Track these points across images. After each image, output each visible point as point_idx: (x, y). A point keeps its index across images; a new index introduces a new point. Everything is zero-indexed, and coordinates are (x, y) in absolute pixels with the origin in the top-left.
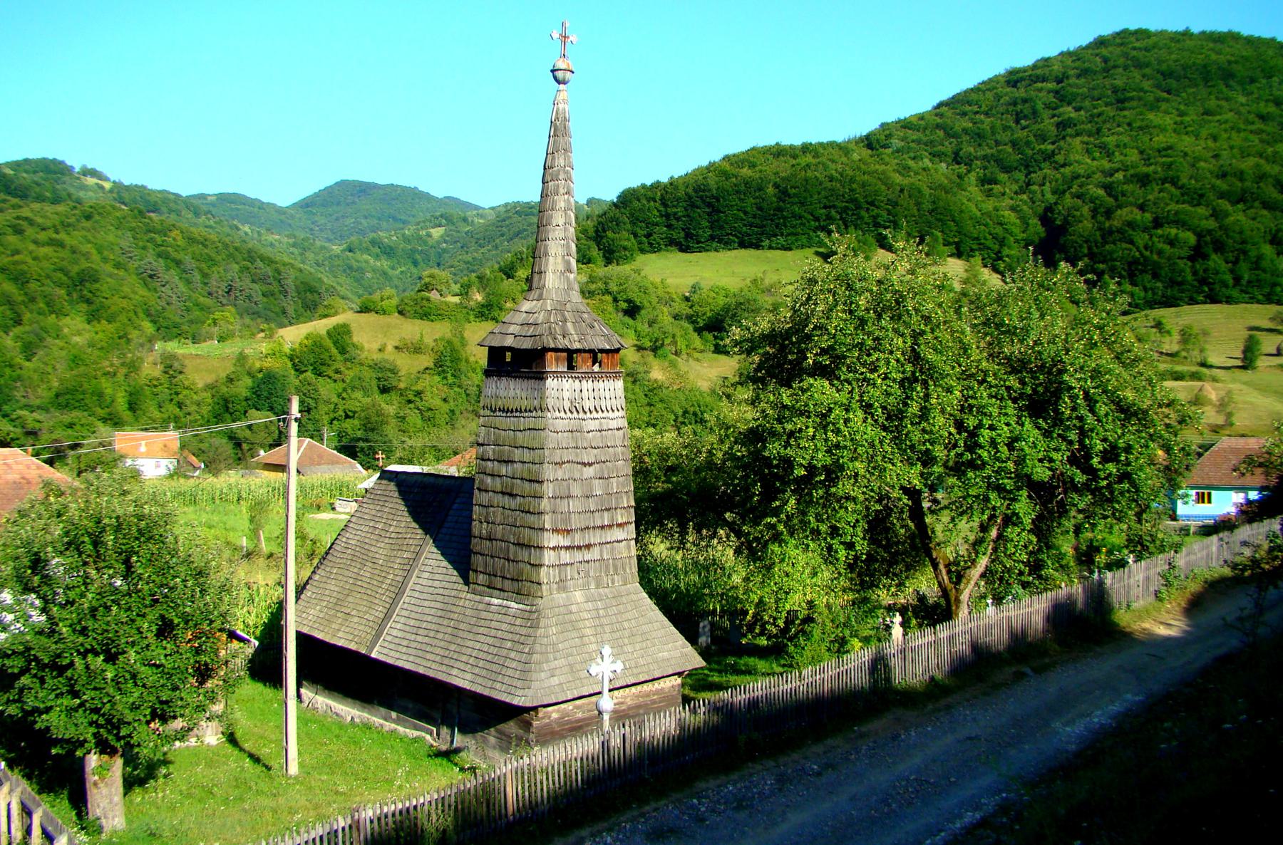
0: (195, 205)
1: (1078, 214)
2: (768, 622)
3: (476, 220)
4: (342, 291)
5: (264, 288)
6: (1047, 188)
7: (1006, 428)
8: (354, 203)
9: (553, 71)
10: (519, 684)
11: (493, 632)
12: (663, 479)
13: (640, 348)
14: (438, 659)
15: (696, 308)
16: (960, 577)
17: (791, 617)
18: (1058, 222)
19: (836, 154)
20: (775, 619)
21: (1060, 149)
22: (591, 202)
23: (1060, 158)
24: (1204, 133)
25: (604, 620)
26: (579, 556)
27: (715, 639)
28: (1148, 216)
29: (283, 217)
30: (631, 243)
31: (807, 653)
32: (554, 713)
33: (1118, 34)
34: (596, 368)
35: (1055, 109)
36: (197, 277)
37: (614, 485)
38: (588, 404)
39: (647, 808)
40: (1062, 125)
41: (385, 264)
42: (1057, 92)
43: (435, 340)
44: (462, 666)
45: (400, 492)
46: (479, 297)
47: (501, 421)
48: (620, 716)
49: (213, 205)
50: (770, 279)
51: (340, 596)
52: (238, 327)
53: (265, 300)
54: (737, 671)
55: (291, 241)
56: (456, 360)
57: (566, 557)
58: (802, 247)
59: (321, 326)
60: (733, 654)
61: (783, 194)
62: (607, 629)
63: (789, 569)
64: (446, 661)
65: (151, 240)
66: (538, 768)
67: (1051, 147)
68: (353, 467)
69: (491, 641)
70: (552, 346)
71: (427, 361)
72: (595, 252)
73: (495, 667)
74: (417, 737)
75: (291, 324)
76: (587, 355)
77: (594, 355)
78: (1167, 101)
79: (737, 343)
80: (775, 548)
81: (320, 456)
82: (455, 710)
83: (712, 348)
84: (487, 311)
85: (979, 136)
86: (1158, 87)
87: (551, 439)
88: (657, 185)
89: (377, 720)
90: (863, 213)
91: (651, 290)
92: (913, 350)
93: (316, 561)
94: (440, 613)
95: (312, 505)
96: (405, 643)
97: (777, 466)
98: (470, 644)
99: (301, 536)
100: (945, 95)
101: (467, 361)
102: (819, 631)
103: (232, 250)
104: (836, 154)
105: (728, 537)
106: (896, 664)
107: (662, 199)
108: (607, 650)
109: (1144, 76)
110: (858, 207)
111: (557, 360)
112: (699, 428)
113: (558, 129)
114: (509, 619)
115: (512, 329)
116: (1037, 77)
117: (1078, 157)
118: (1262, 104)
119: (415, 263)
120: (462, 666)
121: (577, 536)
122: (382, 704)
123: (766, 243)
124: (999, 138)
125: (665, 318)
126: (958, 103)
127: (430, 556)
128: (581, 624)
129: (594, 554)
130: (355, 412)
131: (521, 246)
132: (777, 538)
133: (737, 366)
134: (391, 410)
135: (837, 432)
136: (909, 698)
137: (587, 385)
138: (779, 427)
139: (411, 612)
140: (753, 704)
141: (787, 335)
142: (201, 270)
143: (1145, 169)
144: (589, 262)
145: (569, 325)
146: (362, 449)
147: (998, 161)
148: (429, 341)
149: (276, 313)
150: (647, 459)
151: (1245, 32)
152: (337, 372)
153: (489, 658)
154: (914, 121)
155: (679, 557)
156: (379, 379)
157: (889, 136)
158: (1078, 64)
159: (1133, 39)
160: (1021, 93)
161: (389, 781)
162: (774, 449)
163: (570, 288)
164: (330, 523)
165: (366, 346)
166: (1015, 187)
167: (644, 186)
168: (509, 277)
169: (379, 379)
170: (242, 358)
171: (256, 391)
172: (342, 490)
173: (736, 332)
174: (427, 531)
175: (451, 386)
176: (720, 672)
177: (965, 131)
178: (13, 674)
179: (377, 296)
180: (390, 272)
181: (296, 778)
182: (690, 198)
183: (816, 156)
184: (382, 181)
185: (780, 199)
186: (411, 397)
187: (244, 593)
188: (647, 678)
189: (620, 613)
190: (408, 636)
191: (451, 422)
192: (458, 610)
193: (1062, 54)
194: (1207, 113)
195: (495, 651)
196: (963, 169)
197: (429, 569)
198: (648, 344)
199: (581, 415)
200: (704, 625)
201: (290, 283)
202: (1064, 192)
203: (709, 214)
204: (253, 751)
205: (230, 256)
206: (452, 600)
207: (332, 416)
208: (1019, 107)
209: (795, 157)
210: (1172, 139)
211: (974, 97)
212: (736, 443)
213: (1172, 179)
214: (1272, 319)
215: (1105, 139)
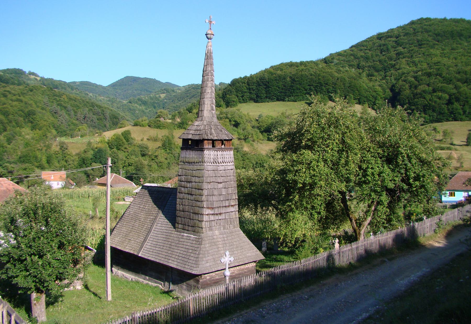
0: (72, 86)
1: (404, 87)
2: (288, 242)
3: (177, 91)
4: (127, 118)
5: (98, 117)
6: (392, 78)
7: (377, 169)
8: (131, 85)
9: (206, 35)
10: (195, 266)
11: (185, 246)
12: (248, 188)
13: (239, 139)
14: (164, 256)
15: (261, 124)
16: (360, 225)
17: (297, 240)
18: (397, 91)
19: (313, 65)
20: (291, 241)
21: (397, 63)
22: (221, 84)
23: (397, 67)
24: (452, 57)
25: (226, 242)
26: (217, 217)
28: (431, 88)
29: (105, 90)
30: (236, 99)
31: (303, 254)
33: (419, 20)
34: (223, 146)
35: (395, 48)
37: (230, 191)
38: (220, 160)
39: (243, 312)
40: (398, 54)
41: (143, 108)
42: (396, 42)
43: (162, 136)
44: (173, 259)
45: (149, 194)
46: (179, 120)
47: (187, 167)
48: (232, 278)
49: (78, 86)
51: (127, 233)
52: (88, 132)
53: (98, 121)
54: (276, 260)
55: (108, 99)
56: (170, 144)
57: (212, 218)
58: (300, 100)
59: (119, 131)
60: (275, 254)
61: (293, 80)
63: (296, 222)
64: (167, 257)
65: (55, 99)
66: (202, 297)
67: (394, 62)
69: (184, 249)
70: (206, 138)
71: (159, 144)
72: (222, 103)
73: (185, 260)
74: (156, 286)
75: (108, 130)
76: (220, 142)
77: (222, 141)
78: (438, 45)
79: (276, 137)
80: (291, 214)
81: (119, 180)
83: (267, 139)
84: (182, 125)
85: (367, 59)
86: (434, 39)
87: (206, 174)
88: (245, 77)
89: (141, 280)
90: (323, 88)
91: (244, 117)
92: (342, 139)
93: (118, 220)
94: (164, 239)
95: (116, 199)
97: (291, 183)
98: (176, 251)
99: (112, 211)
100: (354, 43)
101: (174, 144)
103: (86, 103)
104: (313, 65)
105: (273, 210)
107: (248, 82)
108: (227, 253)
109: (429, 35)
110: (322, 85)
111: (208, 143)
112: (262, 169)
113: (208, 57)
115: (191, 132)
116: (389, 36)
117: (404, 66)
119: (155, 107)
120: (173, 259)
122: (143, 274)
123: (287, 99)
124: (374, 59)
125: (249, 128)
126: (359, 46)
129: (222, 217)
130: (132, 164)
131: (195, 101)
132: (291, 210)
133: (276, 146)
134: (146, 163)
135: (314, 170)
136: (341, 270)
137: (220, 153)
138: (292, 168)
139: (154, 239)
140: (283, 273)
141: (295, 134)
142: (74, 110)
143: (429, 71)
144: (220, 106)
145: (213, 130)
146: (135, 178)
148: (160, 136)
149: (102, 126)
150: (242, 181)
152: (126, 148)
153: (183, 256)
154: (342, 53)
155: (254, 218)
156: (141, 151)
157: (333, 59)
158: (404, 31)
159: (425, 21)
160: (382, 42)
161: (146, 303)
162: (290, 177)
164: (123, 205)
165: (136, 139)
166: (380, 78)
167: (240, 78)
168: (190, 112)
169: (141, 151)
170: (89, 143)
171: (95, 156)
172: (128, 193)
173: (276, 133)
174: (159, 208)
175: (168, 153)
176: (270, 261)
177: (362, 56)
180: (145, 111)
181: (111, 301)
182: (258, 82)
183: (306, 66)
184: (142, 76)
185: (292, 83)
186: (153, 158)
187: (91, 232)
189: (232, 239)
190: (153, 248)
192: (171, 238)
193: (398, 27)
195: (185, 253)
196: (361, 71)
197: (160, 223)
198: (243, 137)
199: (218, 164)
200: (264, 243)
201: (108, 115)
202: (399, 79)
204: (95, 291)
205: (85, 105)
206: (169, 234)
207: (124, 165)
208: (382, 47)
209: (297, 67)
210: (440, 59)
211: (365, 43)
212: (276, 174)
213: (440, 74)
215: (414, 59)
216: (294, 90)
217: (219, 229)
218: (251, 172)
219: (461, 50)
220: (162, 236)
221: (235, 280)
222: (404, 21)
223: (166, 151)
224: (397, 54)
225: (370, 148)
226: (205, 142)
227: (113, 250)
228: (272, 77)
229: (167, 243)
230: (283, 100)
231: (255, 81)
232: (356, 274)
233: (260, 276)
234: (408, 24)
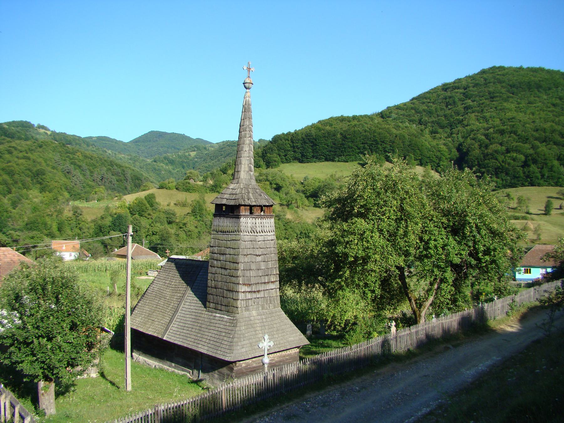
0: (88, 141)
1: (473, 147)
2: (337, 325)
4: (152, 179)
5: (117, 178)
6: (460, 135)
7: (441, 240)
8: (157, 141)
9: (244, 84)
10: (228, 351)
11: (217, 329)
13: (281, 205)
15: (306, 187)
16: (421, 305)
18: (464, 151)
19: (367, 120)
20: (340, 323)
21: (465, 118)
22: (260, 141)
23: (465, 122)
24: (528, 112)
25: (265, 324)
26: (254, 295)
27: (314, 332)
28: (504, 148)
29: (125, 147)
30: (278, 159)
32: (243, 364)
33: (491, 68)
34: (262, 213)
35: (463, 101)
36: (88, 173)
39: (284, 406)
40: (466, 108)
41: (170, 167)
42: (464, 94)
44: (203, 343)
45: (176, 267)
46: (211, 182)
47: (221, 236)
48: (272, 366)
49: (95, 141)
50: (339, 175)
51: (150, 313)
52: (106, 195)
53: (118, 183)
55: (129, 157)
56: (201, 210)
57: (249, 296)
58: (353, 161)
59: (142, 195)
60: (321, 339)
61: (344, 137)
62: (267, 327)
63: (346, 302)
64: (196, 341)
65: (68, 157)
66: (236, 388)
67: (461, 118)
68: (156, 256)
69: (216, 332)
70: (243, 203)
71: (188, 210)
72: (262, 163)
73: (217, 344)
74: (184, 374)
75: (129, 194)
76: (258, 208)
77: (261, 208)
78: (512, 97)
80: (340, 292)
82: (200, 363)
83: (313, 205)
84: (215, 188)
85: (430, 113)
86: (508, 91)
87: (242, 245)
88: (289, 134)
89: (166, 367)
90: (379, 146)
91: (287, 179)
92: (401, 206)
93: (139, 297)
95: (138, 273)
96: (178, 333)
97: (341, 257)
98: (207, 334)
99: (133, 286)
100: (415, 95)
101: (206, 210)
102: (359, 329)
103: (103, 161)
104: (367, 120)
106: (393, 343)
107: (291, 139)
108: (266, 337)
109: (502, 87)
110: (377, 144)
111: (245, 210)
112: (307, 240)
114: (224, 323)
115: (226, 196)
116: (456, 87)
117: (473, 122)
118: (554, 99)
119: (183, 167)
120: (203, 343)
121: (254, 287)
122: (168, 360)
124: (438, 113)
125: (293, 192)
126: (421, 98)
127: (189, 295)
128: (255, 325)
130: (157, 232)
131: (230, 160)
132: (341, 288)
134: (172, 231)
135: (368, 242)
136: (399, 358)
137: (258, 221)
138: (342, 240)
139: (181, 320)
140: (330, 360)
141: (346, 199)
142: (90, 170)
143: (503, 128)
144: (259, 167)
145: (251, 194)
146: (160, 248)
147: (438, 124)
148: (189, 201)
150: (284, 253)
151: (547, 67)
152: (149, 214)
154: (402, 106)
155: (298, 296)
156: (167, 218)
157: (391, 113)
158: (473, 81)
159: (497, 70)
160: (448, 94)
161: (171, 394)
162: (340, 249)
163: (251, 178)
164: (146, 281)
165: (162, 203)
166: (446, 135)
167: (283, 134)
169: (167, 218)
170: (107, 208)
171: (114, 223)
172: (151, 266)
174: (188, 284)
175: (199, 221)
176: (316, 346)
177: (424, 110)
178: (7, 346)
179: (166, 182)
180: (173, 171)
181: (130, 392)
182: (304, 139)
185: (343, 140)
186: (181, 226)
187: (108, 311)
188: (284, 349)
189: (272, 320)
190: (180, 330)
191: (199, 237)
193: (466, 77)
194: (530, 103)
196: (423, 127)
198: (285, 203)
199: (256, 234)
200: (309, 326)
201: (129, 176)
202: (467, 137)
203: (312, 146)
204: (112, 380)
205: (103, 164)
206: (199, 315)
207: (147, 234)
208: (447, 100)
209: (349, 121)
210: (515, 114)
211: (428, 95)
212: (323, 246)
213: (514, 132)
214: (558, 193)
215: (485, 114)
216: (345, 148)
217: (257, 309)
218: (294, 244)
219: (540, 104)
220: (190, 316)
221: (275, 369)
222: (473, 69)
223: (196, 217)
224: (465, 108)
225: (432, 216)
226: (242, 208)
227: (133, 331)
228: (320, 134)
229: (196, 324)
230: (333, 160)
231: (300, 137)
232: (416, 362)
233: (304, 363)
234: (478, 74)
